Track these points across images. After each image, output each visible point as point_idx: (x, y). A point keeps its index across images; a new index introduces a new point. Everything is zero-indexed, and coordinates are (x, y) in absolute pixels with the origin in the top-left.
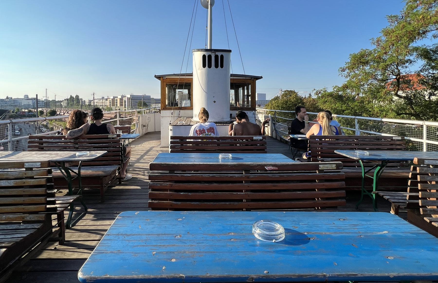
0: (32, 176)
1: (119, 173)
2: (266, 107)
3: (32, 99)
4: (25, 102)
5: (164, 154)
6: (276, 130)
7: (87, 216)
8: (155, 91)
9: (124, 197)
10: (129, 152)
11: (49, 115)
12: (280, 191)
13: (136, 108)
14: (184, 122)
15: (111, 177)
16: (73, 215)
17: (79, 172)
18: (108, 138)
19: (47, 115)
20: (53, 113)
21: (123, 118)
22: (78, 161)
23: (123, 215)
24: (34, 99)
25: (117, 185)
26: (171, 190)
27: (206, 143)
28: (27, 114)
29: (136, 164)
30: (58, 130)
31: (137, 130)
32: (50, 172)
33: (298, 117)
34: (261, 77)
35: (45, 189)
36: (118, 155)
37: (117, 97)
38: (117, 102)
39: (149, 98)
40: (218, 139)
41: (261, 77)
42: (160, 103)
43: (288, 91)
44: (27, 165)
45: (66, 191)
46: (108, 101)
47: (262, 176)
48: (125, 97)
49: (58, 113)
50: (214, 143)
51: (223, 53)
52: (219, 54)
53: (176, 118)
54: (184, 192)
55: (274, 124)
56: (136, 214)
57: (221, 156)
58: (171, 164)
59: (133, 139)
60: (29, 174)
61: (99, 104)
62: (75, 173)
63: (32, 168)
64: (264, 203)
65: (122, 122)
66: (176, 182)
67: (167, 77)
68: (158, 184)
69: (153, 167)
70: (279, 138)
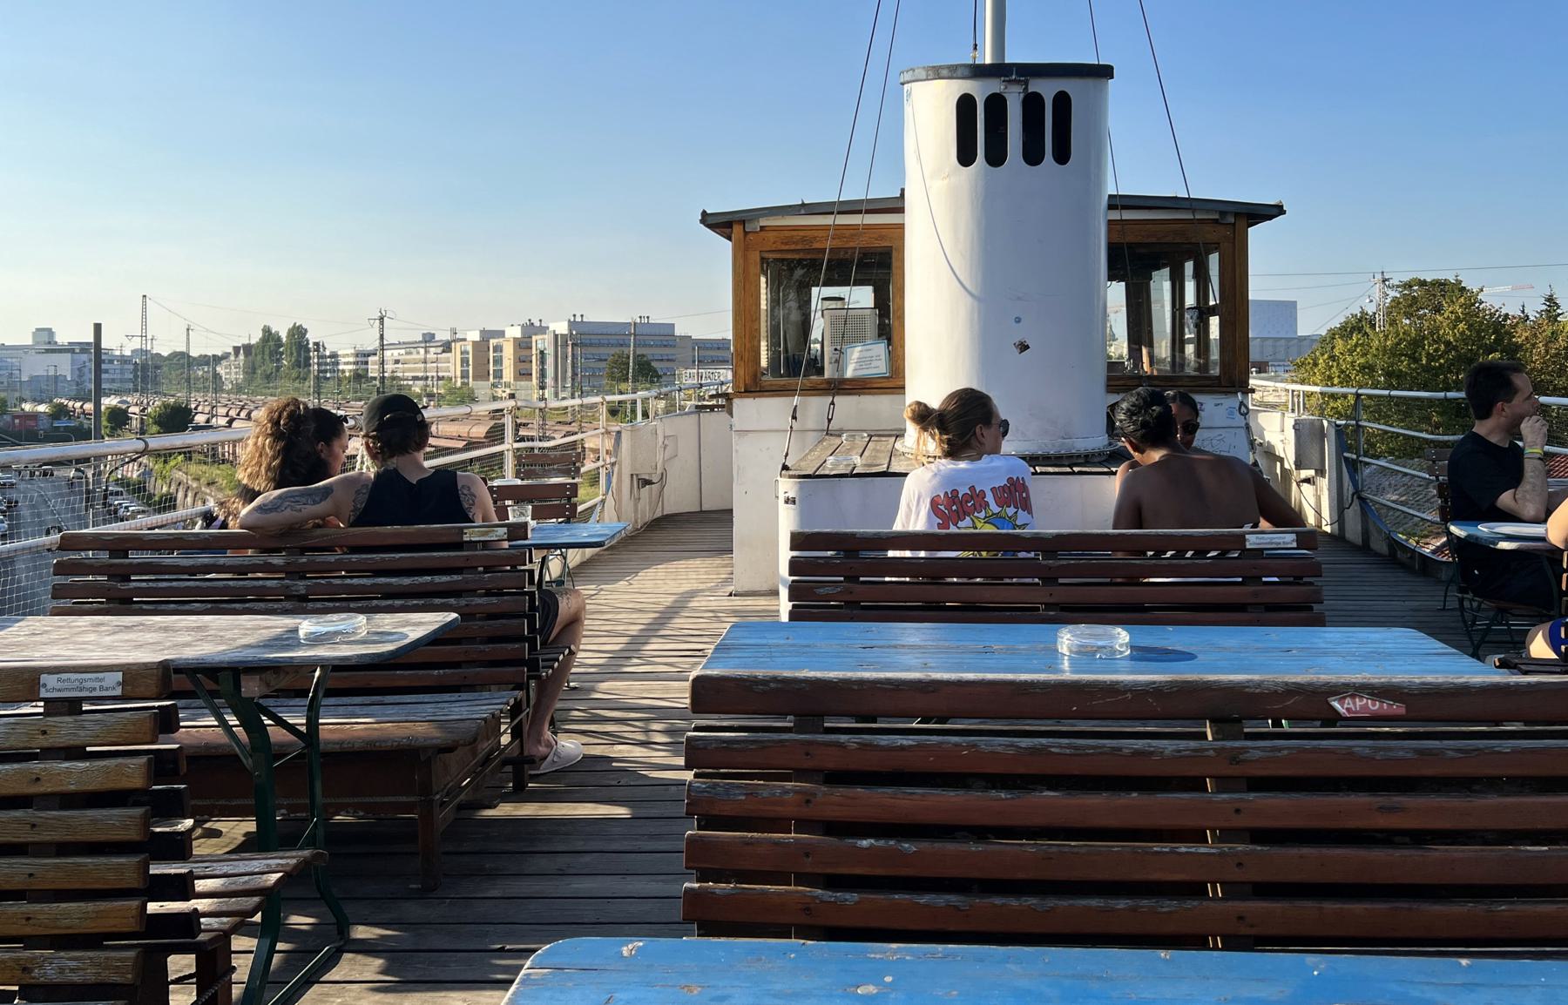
0: (78, 742)
1: (517, 733)
2: (1302, 374)
3: (70, 349)
4: (39, 367)
5: (750, 628)
6: (1362, 500)
7: (351, 967)
8: (699, 297)
9: (543, 863)
10: (574, 621)
11: (155, 428)
12: (1420, 838)
13: (599, 391)
14: (858, 460)
15: (474, 754)
16: (276, 958)
17: (312, 723)
18: (460, 546)
19: (143, 432)
20: (176, 419)
21: (532, 439)
22: (308, 666)
23: (557, 961)
24: (84, 348)
25: (507, 798)
26: (804, 825)
27: (986, 573)
28: (44, 424)
29: (604, 686)
30: (200, 508)
31: (610, 502)
32: (166, 722)
33: (1482, 428)
34: (1278, 210)
35: (138, 811)
36: (515, 636)
37: (501, 334)
38: (499, 361)
39: (664, 336)
40: (1037, 542)
41: (1278, 210)
42: (725, 362)
43: (1422, 283)
44: (52, 686)
45: (238, 829)
46: (455, 357)
47: (1314, 750)
48: (543, 330)
49: (200, 419)
50: (1028, 568)
51: (1069, 85)
52: (1047, 89)
53: (812, 438)
54: (876, 836)
55: (1353, 466)
56: (625, 951)
57: (1067, 639)
58: (806, 681)
59: (589, 552)
60: (65, 730)
61: (407, 369)
62: (291, 728)
63: (79, 701)
64: (1330, 906)
65: (529, 462)
66: (835, 778)
67: (763, 222)
68: (738, 792)
69: (707, 694)
70: (1379, 545)
